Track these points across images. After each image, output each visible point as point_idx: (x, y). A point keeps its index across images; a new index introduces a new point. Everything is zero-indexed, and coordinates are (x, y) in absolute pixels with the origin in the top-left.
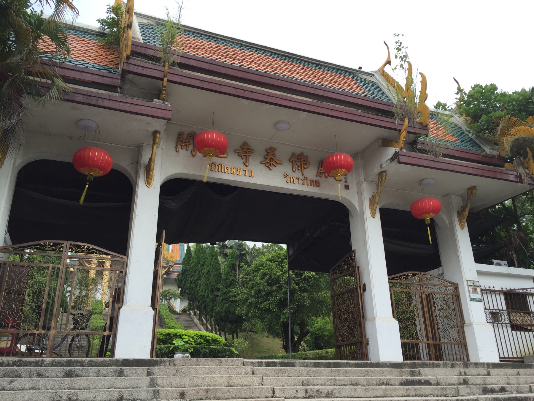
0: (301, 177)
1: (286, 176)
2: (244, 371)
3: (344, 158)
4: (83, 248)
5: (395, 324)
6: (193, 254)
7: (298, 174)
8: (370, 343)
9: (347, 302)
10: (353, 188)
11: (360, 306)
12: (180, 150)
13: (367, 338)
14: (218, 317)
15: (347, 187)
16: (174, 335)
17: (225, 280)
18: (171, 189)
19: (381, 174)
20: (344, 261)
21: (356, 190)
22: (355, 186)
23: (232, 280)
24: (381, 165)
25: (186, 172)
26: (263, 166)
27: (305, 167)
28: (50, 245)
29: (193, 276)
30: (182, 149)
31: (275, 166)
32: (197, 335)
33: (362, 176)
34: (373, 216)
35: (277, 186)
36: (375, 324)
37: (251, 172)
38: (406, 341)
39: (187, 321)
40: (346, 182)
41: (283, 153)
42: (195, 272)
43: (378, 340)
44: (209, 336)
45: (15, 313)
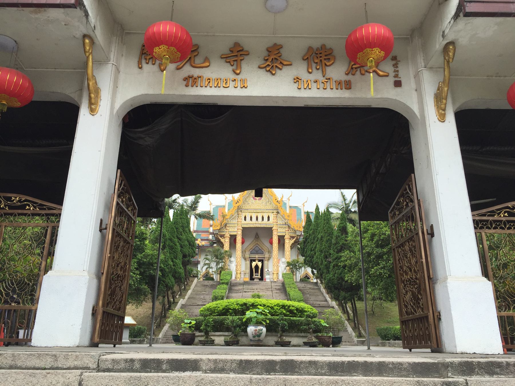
0: (321, 79)
1: (297, 80)
2: (62, 380)
3: (373, 30)
4: (14, 200)
5: (486, 289)
6: (313, 220)
7: (317, 75)
8: (443, 318)
9: (408, 256)
10: (409, 84)
11: (424, 260)
12: (145, 65)
13: (439, 309)
14: (330, 284)
15: (398, 84)
16: (251, 306)
17: (335, 244)
18: (138, 121)
19: (446, 49)
20: (402, 195)
21: (413, 85)
22: (413, 80)
23: (343, 244)
24: (444, 32)
25: (151, 92)
26: (262, 72)
27: (328, 64)
28: (29, 206)
29: (312, 243)
30: (147, 63)
31: (281, 69)
32: (278, 305)
33: (421, 62)
34: (442, 118)
35: (283, 95)
36: (446, 286)
37: (243, 81)
38: (503, 313)
39: (313, 289)
40: (396, 76)
41: (293, 48)
42: (314, 239)
43: (453, 312)
44: (293, 306)
45: (9, 284)
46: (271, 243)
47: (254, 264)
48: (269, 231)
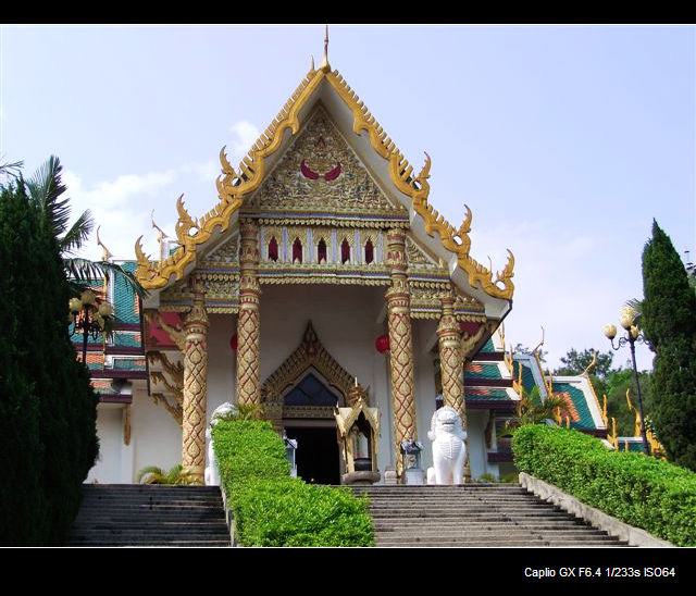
46: (383, 345)
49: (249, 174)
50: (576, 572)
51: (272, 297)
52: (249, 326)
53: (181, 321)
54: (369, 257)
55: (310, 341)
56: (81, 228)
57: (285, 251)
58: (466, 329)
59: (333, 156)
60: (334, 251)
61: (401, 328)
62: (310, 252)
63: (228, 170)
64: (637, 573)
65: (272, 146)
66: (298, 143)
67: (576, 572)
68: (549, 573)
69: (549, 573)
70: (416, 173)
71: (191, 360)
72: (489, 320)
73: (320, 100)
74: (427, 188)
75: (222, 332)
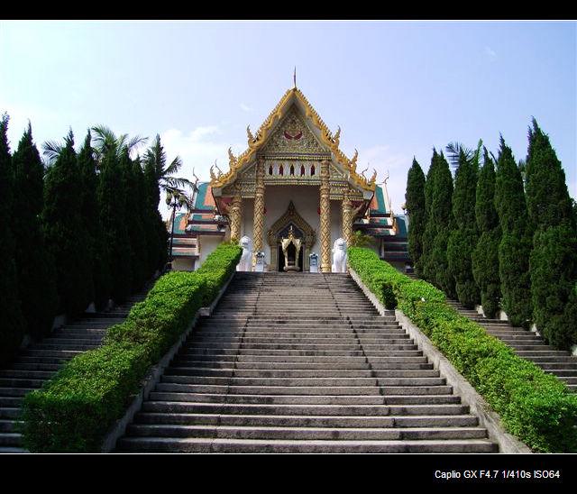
47: (285, 243)
48: (315, 190)
49: (260, 138)
50: (478, 474)
51: (271, 191)
52: (259, 203)
53: (230, 202)
54: (313, 173)
55: (291, 209)
56: (175, 165)
57: (276, 170)
58: (354, 204)
59: (299, 128)
60: (297, 170)
61: (325, 204)
62: (287, 171)
63: (250, 136)
64: (528, 475)
65: (270, 125)
66: (283, 122)
67: (478, 474)
68: (455, 475)
69: (455, 475)
70: (333, 136)
71: (234, 218)
72: (365, 200)
73: (294, 104)
74: (338, 142)
75: (248, 205)
